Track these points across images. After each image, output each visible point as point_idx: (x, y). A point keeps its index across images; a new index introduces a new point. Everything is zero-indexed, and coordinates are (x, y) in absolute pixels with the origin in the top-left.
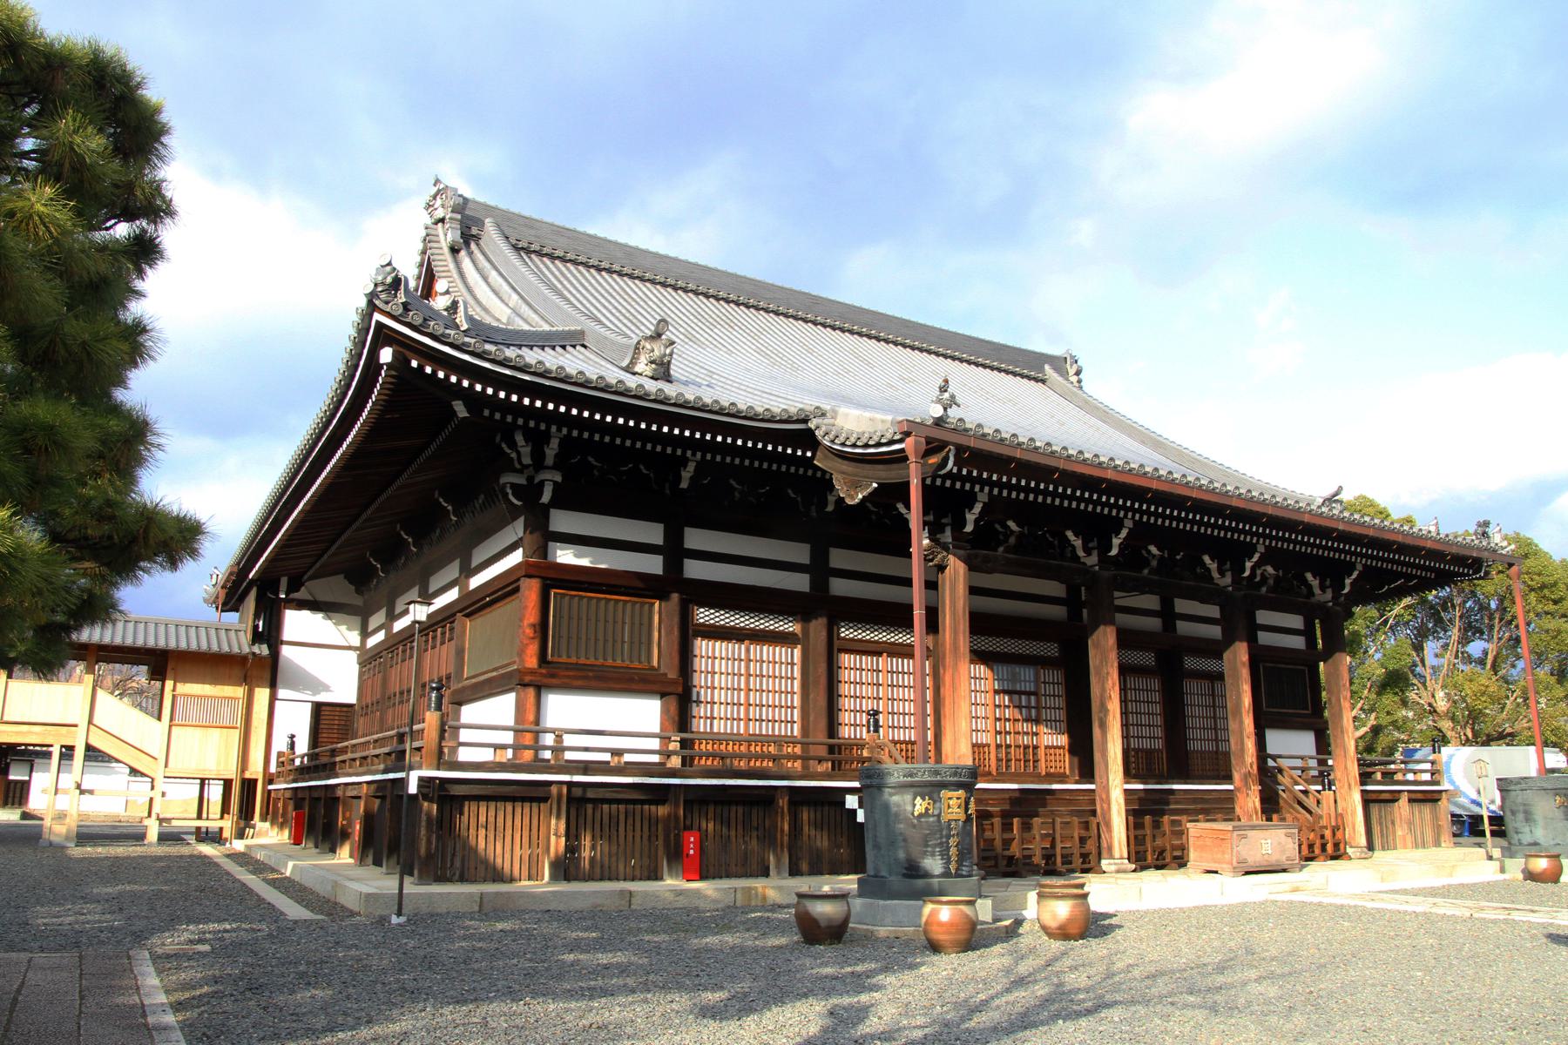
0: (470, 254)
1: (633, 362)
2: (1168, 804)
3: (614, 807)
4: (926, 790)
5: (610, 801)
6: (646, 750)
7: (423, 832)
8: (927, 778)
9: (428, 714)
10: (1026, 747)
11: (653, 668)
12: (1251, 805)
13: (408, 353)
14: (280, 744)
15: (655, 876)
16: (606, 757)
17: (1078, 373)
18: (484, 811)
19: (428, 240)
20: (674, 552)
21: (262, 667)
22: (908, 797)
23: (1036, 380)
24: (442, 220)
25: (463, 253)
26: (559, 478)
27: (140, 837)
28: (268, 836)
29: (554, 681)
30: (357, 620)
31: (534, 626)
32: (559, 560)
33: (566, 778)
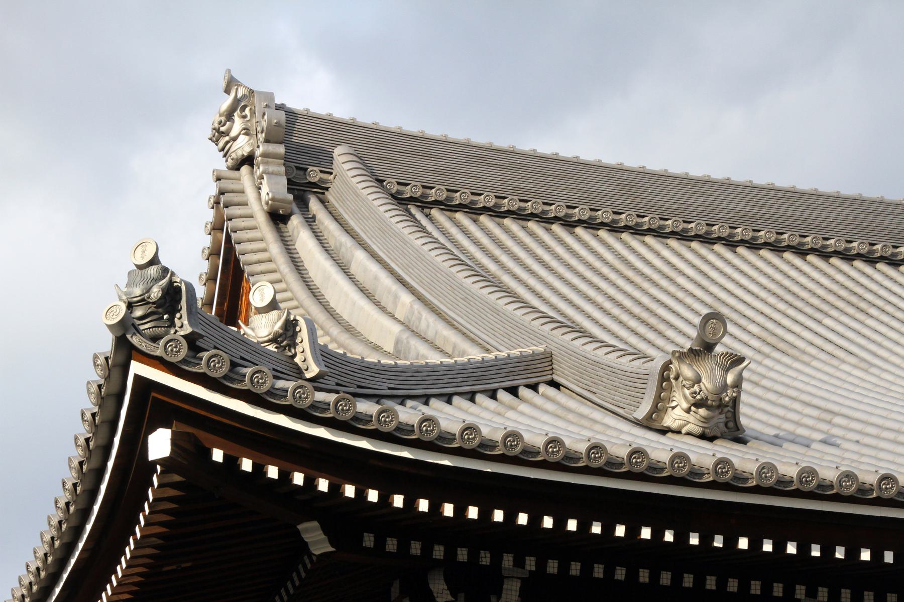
0: (310, 221)
1: (659, 407)
24: (249, 160)
25: (295, 221)
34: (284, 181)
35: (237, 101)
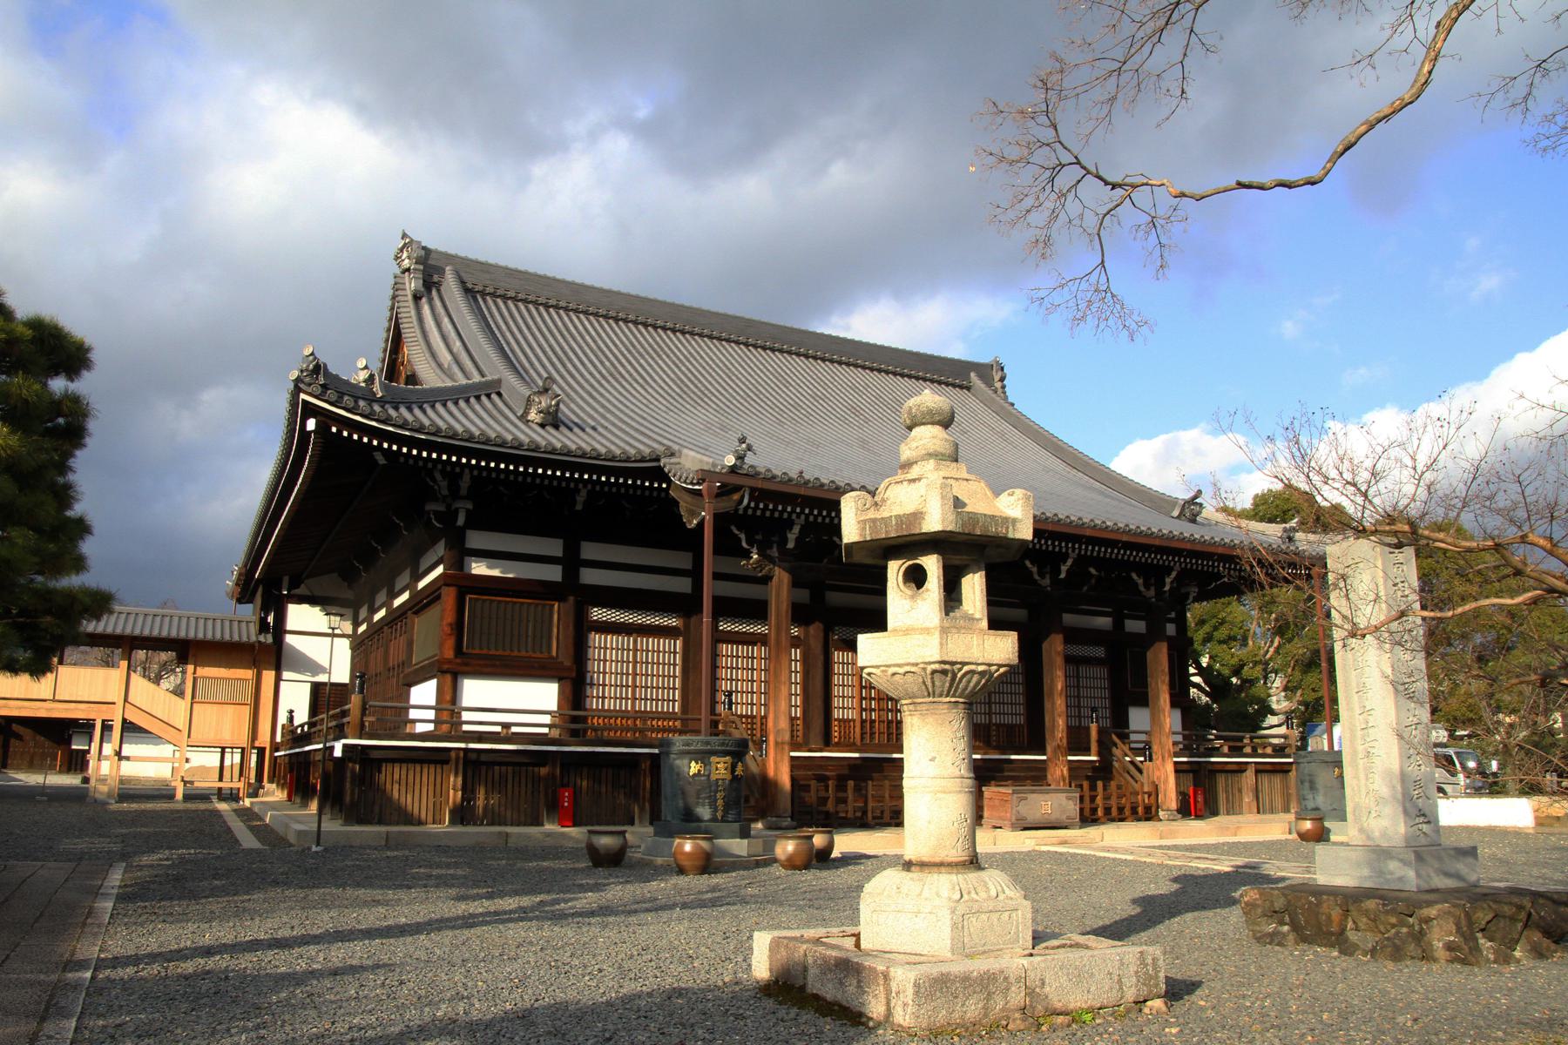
0: (430, 301)
1: (526, 412)
2: (1002, 771)
5: (500, 764)
6: (540, 724)
7: (348, 785)
8: (699, 747)
10: (890, 722)
12: (1058, 773)
14: (282, 719)
15: (537, 822)
16: (498, 729)
17: (1002, 379)
18: (397, 771)
19: (397, 287)
20: (572, 562)
21: (271, 653)
22: (686, 761)
23: (961, 387)
24: (408, 270)
26: (470, 506)
27: (171, 796)
28: (274, 794)
30: (349, 612)
33: (462, 745)
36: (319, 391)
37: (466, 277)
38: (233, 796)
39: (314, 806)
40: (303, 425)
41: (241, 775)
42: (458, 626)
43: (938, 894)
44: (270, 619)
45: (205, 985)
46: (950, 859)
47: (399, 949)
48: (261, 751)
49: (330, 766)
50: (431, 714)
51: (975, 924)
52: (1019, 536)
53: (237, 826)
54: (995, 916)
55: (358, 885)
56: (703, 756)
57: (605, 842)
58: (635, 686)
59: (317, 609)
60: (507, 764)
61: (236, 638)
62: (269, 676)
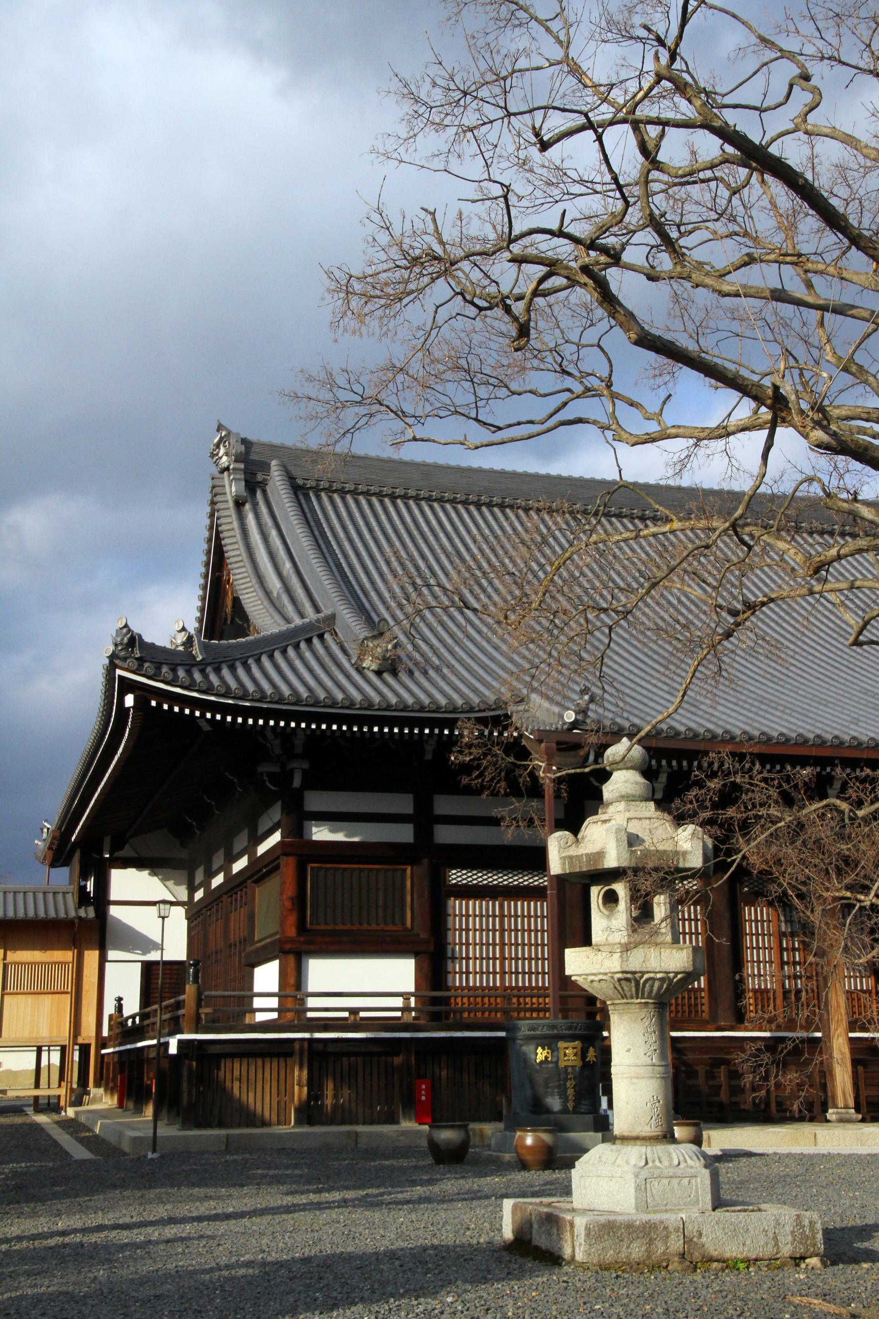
1: (360, 659)
3: (353, 1059)
4: (539, 1041)
7: (185, 1085)
8: (546, 1031)
9: (187, 987)
11: (406, 930)
13: (148, 695)
14: (109, 1008)
15: (392, 1119)
16: (346, 1014)
18: (238, 1067)
20: (424, 820)
21: (92, 929)
22: (532, 1047)
24: (227, 469)
25: (248, 506)
26: (306, 766)
28: (102, 1100)
29: (311, 947)
30: (184, 874)
31: (292, 899)
32: (315, 838)
33: (307, 1035)
34: (243, 483)
35: (221, 438)
36: (135, 665)
37: (295, 472)
38: (52, 1106)
39: (149, 1111)
40: (121, 701)
41: (61, 1078)
42: (300, 901)
43: (627, 1162)
44: (90, 886)
45: (67, 1251)
46: (644, 1134)
47: (221, 1227)
48: (85, 1050)
49: (165, 1064)
50: (274, 1002)
51: (657, 1187)
52: (688, 865)
53: (64, 1139)
54: (675, 1182)
55: (194, 1185)
56: (549, 1041)
57: (447, 1135)
58: (503, 959)
59: (146, 873)
60: (356, 1054)
61: (52, 914)
62: (91, 957)
